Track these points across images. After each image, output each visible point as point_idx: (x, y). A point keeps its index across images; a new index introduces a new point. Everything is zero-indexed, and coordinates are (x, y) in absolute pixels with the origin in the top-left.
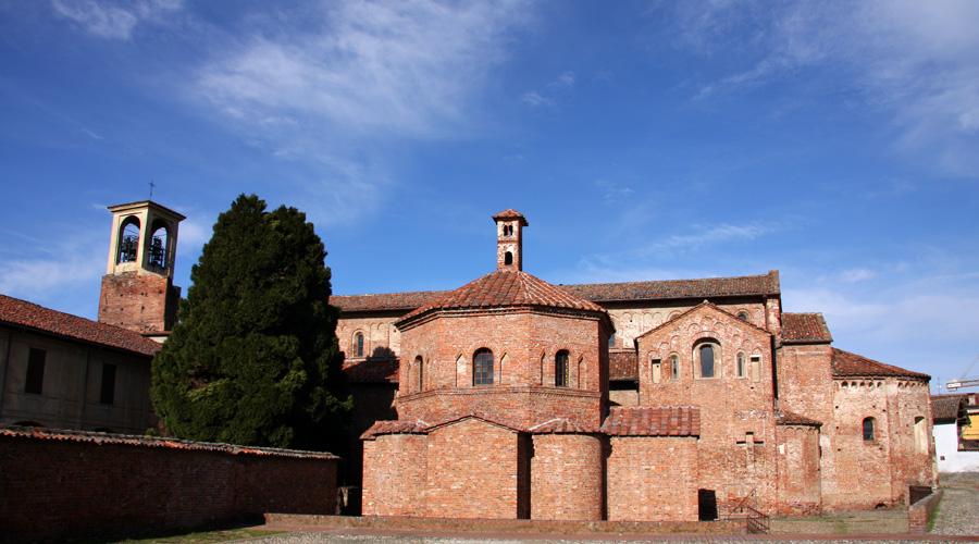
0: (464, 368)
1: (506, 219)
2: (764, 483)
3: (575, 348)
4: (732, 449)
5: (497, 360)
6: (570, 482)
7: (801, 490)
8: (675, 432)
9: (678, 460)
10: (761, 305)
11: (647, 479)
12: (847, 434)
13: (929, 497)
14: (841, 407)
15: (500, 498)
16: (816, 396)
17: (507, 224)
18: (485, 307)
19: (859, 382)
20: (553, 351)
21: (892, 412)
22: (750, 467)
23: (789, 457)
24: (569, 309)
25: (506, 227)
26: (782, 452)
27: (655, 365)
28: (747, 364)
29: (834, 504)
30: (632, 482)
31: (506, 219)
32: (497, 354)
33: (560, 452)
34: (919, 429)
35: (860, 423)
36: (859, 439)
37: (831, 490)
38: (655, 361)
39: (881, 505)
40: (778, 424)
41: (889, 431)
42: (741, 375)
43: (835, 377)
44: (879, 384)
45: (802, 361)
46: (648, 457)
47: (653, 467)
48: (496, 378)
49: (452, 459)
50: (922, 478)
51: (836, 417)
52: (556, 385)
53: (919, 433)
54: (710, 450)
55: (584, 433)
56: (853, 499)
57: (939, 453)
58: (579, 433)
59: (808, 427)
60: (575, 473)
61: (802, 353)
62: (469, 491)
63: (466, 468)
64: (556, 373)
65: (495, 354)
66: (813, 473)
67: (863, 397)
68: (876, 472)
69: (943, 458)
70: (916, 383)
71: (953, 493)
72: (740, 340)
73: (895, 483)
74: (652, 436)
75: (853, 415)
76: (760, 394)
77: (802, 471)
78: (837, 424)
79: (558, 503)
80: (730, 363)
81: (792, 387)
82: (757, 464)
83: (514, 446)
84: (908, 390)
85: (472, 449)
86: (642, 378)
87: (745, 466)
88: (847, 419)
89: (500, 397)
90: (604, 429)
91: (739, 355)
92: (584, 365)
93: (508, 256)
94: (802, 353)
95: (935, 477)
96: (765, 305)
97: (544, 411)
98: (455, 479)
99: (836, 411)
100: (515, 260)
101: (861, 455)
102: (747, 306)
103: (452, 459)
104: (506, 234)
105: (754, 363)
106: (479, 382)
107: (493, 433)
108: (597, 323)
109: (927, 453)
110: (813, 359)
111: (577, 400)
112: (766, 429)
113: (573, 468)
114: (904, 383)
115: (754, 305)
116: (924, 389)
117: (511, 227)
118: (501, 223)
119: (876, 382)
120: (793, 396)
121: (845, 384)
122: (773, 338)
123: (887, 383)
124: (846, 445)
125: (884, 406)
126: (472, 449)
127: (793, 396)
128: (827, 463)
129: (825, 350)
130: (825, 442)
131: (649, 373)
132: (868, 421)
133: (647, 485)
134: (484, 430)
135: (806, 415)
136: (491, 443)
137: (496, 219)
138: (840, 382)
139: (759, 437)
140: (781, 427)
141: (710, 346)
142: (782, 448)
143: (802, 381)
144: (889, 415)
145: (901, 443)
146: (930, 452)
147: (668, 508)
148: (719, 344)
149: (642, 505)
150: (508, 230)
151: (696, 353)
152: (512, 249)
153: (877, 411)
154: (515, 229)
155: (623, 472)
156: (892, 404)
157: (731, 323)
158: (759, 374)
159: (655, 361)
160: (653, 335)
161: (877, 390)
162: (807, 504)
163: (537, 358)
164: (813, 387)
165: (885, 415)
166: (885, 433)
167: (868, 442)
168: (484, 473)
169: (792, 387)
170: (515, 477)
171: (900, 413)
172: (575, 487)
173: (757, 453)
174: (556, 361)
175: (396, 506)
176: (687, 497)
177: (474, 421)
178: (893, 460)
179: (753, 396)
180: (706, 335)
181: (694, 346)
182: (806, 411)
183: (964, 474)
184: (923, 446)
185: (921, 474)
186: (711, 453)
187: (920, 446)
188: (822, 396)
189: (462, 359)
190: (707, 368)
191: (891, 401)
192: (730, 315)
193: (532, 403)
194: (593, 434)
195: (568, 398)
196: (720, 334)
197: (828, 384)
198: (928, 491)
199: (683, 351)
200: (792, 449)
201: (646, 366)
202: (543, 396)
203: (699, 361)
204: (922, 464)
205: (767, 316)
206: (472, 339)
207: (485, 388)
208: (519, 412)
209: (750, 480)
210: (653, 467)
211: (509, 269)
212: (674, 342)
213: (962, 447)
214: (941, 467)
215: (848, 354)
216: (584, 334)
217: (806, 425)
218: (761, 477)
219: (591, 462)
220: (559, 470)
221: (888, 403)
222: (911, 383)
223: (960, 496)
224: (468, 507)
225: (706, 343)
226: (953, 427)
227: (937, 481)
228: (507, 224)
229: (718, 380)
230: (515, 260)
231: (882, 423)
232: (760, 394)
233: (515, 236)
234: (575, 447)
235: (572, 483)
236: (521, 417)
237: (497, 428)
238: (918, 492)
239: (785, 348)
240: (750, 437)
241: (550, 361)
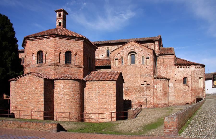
0: (34, 58)
1: (59, 11)
2: (149, 97)
3: (74, 50)
4: (140, 87)
5: (44, 55)
6: (66, 97)
7: (162, 99)
8: (108, 79)
9: (109, 89)
10: (153, 44)
11: (98, 96)
12: (178, 82)
13: (202, 101)
14: (176, 74)
15: (38, 102)
16: (169, 71)
17: (60, 13)
18: (40, 36)
19: (183, 66)
20: (65, 51)
21: (192, 76)
22: (145, 92)
23: (158, 89)
24: (70, 36)
25: (59, 14)
26: (156, 87)
27: (116, 61)
28: (145, 60)
29: (173, 103)
30: (93, 97)
31: (59, 11)
32: (44, 53)
33: (62, 86)
34: (201, 81)
35: (182, 79)
36: (182, 84)
37: (172, 99)
38: (116, 59)
39: (187, 103)
40: (155, 79)
41: (191, 81)
42: (143, 63)
43: (175, 65)
44: (189, 67)
45: (165, 60)
46: (99, 89)
47: (100, 92)
48: (44, 61)
49: (24, 89)
50: (201, 96)
51: (175, 77)
52: (66, 63)
53: (201, 82)
54: (133, 87)
55: (75, 80)
56: (179, 102)
57: (206, 88)
58: (69, 79)
59: (164, 80)
60: (68, 94)
61: (165, 58)
62: (29, 100)
63: (28, 92)
64: (65, 59)
65: (44, 52)
66: (166, 94)
67: (184, 71)
68: (186, 93)
69: (208, 90)
70: (201, 67)
71: (209, 100)
72: (143, 52)
73: (192, 97)
74: (100, 81)
75: (180, 76)
76: (149, 69)
77: (162, 93)
78: (175, 79)
79: (62, 105)
80: (139, 59)
81: (162, 68)
82: (148, 91)
83: (43, 84)
84: (198, 69)
85: (30, 85)
86: (112, 65)
87: (144, 92)
88: (179, 78)
89: (46, 67)
90: (84, 79)
91: (143, 57)
92: (77, 56)
93: (60, 23)
94: (165, 58)
95: (204, 95)
96: (154, 43)
97: (61, 72)
98: (25, 96)
99: (175, 75)
100: (62, 25)
101: (182, 89)
102: (149, 44)
103: (24, 89)
104: (59, 16)
105: (147, 60)
106: (39, 63)
107: (36, 79)
108: (83, 42)
109: (203, 88)
110: (169, 60)
111: (74, 69)
112: (150, 80)
113: (67, 92)
114: (197, 67)
115: (151, 44)
116: (202, 69)
117: (61, 14)
118: (58, 13)
119: (188, 67)
120: (162, 71)
121: (178, 67)
122: (154, 52)
123: (191, 67)
124: (178, 86)
125: (190, 74)
126: (30, 85)
127: (162, 71)
128: (171, 91)
129: (173, 56)
130: (171, 85)
131: (114, 63)
132: (185, 78)
133: (98, 98)
134: (33, 78)
135: (166, 77)
136: (35, 83)
137: (56, 11)
138: (177, 67)
139: (148, 83)
140: (155, 80)
141: (134, 54)
142: (155, 86)
143: (165, 66)
144: (191, 77)
145: (195, 85)
146: (203, 88)
147: (105, 106)
148: (136, 53)
149: (97, 105)
150: (60, 15)
151: (129, 56)
152: (61, 21)
153: (188, 75)
154: (62, 14)
155: (90, 94)
156: (193, 73)
157: (140, 47)
158: (150, 63)
159: (116, 59)
160: (115, 51)
161: (188, 69)
162: (163, 104)
163: (58, 53)
164: (168, 68)
165: (190, 76)
166: (190, 82)
167: (185, 85)
168: (33, 93)
169: (162, 68)
170: (43, 95)
171: (195, 76)
172: (68, 99)
173: (148, 88)
174: (66, 55)
175: (13, 105)
176: (112, 103)
177: (30, 75)
178: (192, 90)
179: (147, 70)
180: (132, 51)
181: (128, 54)
182: (166, 75)
183: (213, 94)
184: (202, 86)
185: (200, 94)
186: (133, 88)
187: (201, 86)
188: (171, 71)
189: (34, 55)
190: (133, 62)
191: (192, 72)
192: (144, 46)
193: (55, 69)
194: (77, 80)
195: (70, 68)
196: (136, 50)
197: (173, 67)
198: (201, 99)
199: (125, 56)
200: (159, 86)
201: (113, 61)
202: (60, 67)
203: (130, 59)
204: (201, 91)
205: (155, 46)
206: (36, 48)
207: (40, 64)
208: (51, 72)
209: (145, 96)
210: (100, 92)
211: (60, 27)
212: (122, 53)
213: (213, 86)
214: (207, 92)
215: (180, 59)
216: (77, 46)
217: (164, 79)
218: (149, 95)
219: (74, 90)
220: (62, 93)
221: (191, 73)
222: (199, 67)
223: (211, 101)
224: (29, 106)
225: (132, 53)
226: (211, 81)
227: (205, 96)
228: (60, 13)
229: (136, 65)
230: (62, 25)
231: (189, 79)
232: (149, 69)
233: (62, 17)
234: (68, 84)
235: (67, 97)
236: (51, 75)
237: (37, 78)
238: (199, 100)
239: (160, 56)
240: (145, 83)
241: (63, 55)
